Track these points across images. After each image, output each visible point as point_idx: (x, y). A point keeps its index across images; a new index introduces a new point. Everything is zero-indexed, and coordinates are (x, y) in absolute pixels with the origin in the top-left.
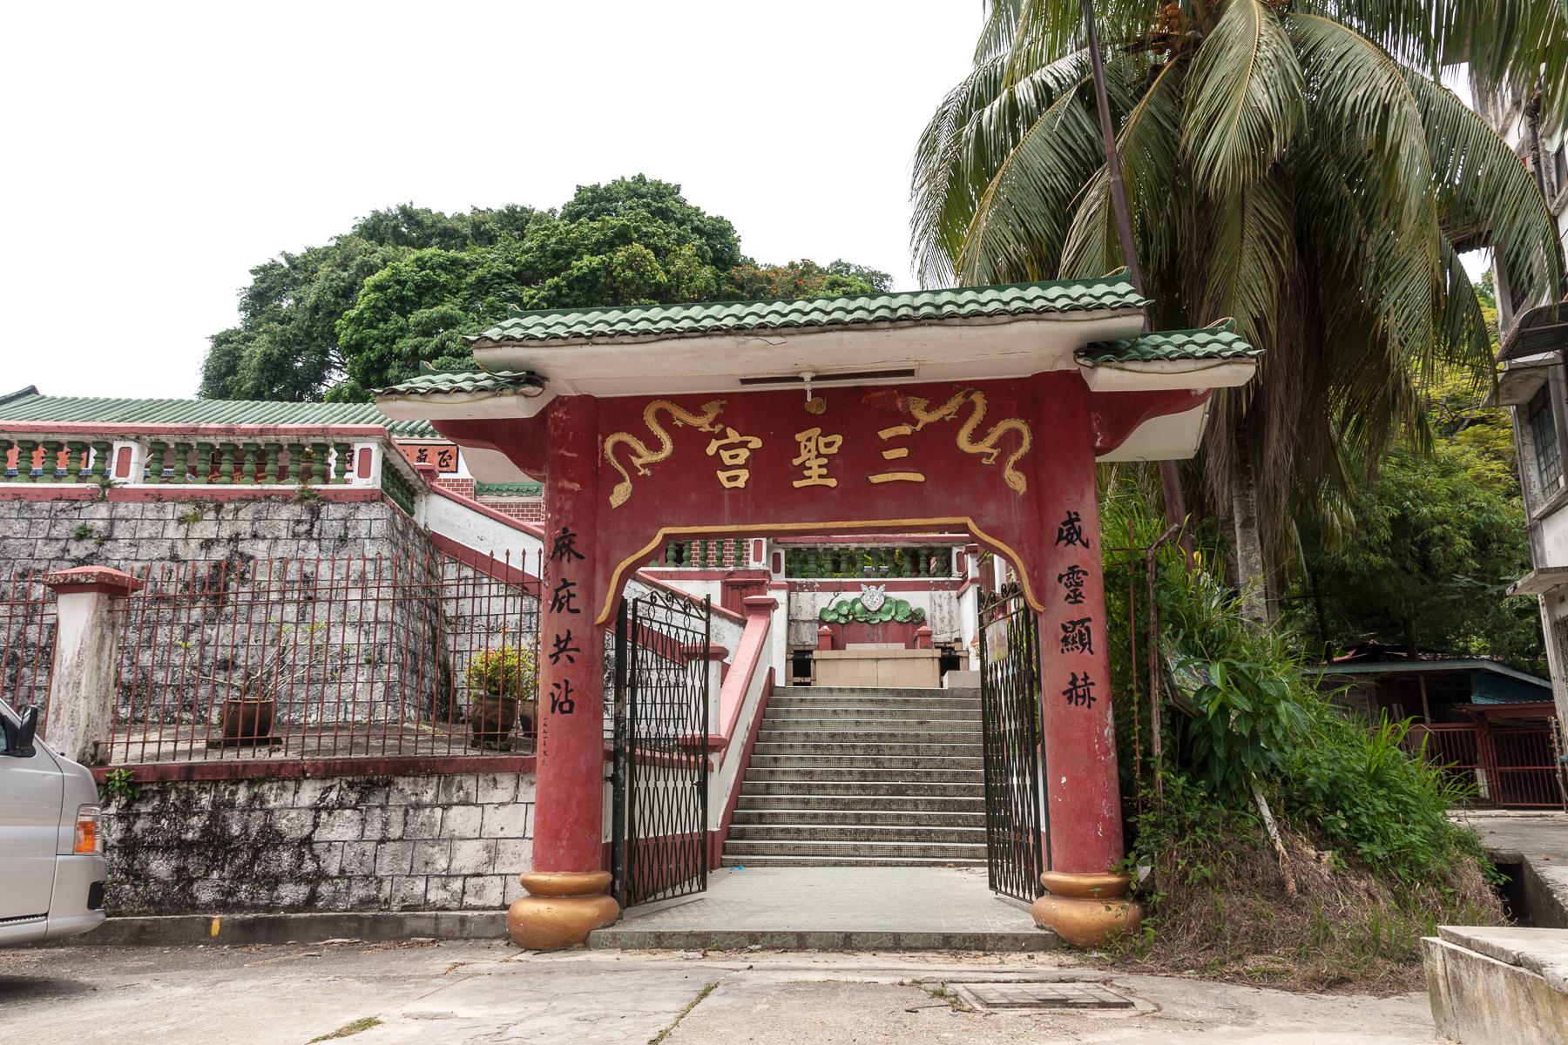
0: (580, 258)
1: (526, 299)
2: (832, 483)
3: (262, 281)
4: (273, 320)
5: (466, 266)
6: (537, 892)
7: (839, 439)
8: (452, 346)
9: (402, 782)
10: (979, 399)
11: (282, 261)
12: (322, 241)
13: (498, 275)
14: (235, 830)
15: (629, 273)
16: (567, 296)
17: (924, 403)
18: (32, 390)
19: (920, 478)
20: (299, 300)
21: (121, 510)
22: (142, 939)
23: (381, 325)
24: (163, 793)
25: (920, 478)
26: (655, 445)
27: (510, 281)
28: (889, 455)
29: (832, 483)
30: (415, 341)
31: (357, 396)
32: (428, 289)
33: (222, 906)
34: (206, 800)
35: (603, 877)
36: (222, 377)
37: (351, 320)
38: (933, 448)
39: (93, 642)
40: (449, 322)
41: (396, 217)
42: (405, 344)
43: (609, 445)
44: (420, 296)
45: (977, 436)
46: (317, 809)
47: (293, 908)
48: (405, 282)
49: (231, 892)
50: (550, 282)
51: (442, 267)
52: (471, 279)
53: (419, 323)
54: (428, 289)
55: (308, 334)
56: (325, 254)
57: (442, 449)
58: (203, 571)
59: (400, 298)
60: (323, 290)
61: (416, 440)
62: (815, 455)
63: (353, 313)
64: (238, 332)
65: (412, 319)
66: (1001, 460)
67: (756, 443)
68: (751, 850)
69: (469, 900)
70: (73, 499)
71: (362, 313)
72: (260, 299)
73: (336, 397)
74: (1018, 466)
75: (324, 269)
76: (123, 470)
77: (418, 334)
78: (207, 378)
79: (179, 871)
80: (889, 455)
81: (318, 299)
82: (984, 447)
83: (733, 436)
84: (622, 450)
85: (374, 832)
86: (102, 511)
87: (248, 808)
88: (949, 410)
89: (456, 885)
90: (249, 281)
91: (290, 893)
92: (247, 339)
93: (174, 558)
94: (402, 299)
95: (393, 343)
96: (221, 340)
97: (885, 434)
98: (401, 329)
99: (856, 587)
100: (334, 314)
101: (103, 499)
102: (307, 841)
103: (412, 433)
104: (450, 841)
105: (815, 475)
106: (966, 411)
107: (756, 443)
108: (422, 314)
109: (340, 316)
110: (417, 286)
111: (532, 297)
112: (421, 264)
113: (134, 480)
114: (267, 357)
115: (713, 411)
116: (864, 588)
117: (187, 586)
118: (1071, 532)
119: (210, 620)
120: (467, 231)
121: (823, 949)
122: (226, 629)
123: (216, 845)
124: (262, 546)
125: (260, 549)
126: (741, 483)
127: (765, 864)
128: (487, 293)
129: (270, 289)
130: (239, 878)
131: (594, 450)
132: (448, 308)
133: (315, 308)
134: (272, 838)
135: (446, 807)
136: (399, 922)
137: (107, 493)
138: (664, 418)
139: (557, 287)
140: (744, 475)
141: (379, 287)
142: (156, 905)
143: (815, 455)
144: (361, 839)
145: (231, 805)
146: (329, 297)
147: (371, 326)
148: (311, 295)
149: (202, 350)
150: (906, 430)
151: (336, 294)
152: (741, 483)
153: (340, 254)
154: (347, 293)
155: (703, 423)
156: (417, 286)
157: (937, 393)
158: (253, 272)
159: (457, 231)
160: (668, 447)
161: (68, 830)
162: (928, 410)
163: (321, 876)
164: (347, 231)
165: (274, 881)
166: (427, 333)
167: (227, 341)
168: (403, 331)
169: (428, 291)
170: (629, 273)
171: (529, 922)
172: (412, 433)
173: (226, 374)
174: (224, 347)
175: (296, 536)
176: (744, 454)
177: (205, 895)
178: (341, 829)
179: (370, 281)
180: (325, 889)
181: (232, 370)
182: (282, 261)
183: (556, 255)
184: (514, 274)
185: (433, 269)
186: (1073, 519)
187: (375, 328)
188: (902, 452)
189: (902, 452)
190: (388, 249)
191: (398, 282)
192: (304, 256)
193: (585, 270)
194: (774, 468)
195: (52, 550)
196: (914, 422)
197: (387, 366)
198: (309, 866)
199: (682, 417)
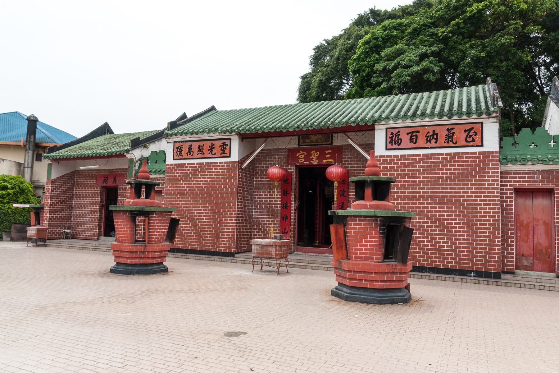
0: (471, 6)
3: (318, 52)
4: (322, 67)
5: (405, 26)
11: (324, 43)
12: (338, 32)
13: (424, 25)
15: (503, 8)
16: (463, 28)
18: (213, 108)
20: (331, 57)
23: (368, 60)
27: (430, 27)
28: (327, 156)
30: (385, 64)
31: (359, 94)
32: (388, 40)
36: (305, 91)
37: (355, 60)
40: (400, 53)
41: (368, 15)
42: (379, 66)
48: (378, 38)
50: (453, 23)
51: (394, 28)
52: (410, 30)
53: (386, 55)
54: (388, 40)
56: (341, 36)
57: (468, 127)
59: (375, 47)
60: (341, 50)
61: (445, 121)
63: (355, 57)
64: (310, 73)
65: (383, 54)
71: (359, 56)
72: (317, 60)
73: (350, 96)
75: (340, 43)
77: (385, 61)
78: (300, 93)
80: (327, 156)
81: (340, 54)
90: (312, 53)
92: (313, 76)
94: (377, 46)
95: (374, 66)
96: (304, 78)
97: (327, 152)
98: (377, 60)
100: (345, 59)
107: (306, 154)
109: (349, 59)
110: (383, 39)
111: (443, 32)
112: (385, 28)
114: (321, 81)
120: (400, 13)
128: (418, 35)
129: (321, 54)
132: (400, 46)
133: (338, 59)
139: (457, 24)
141: (366, 43)
147: (364, 60)
148: (336, 54)
149: (298, 82)
151: (347, 51)
153: (348, 34)
154: (351, 49)
156: (383, 39)
158: (314, 49)
164: (348, 26)
167: (306, 78)
168: (378, 61)
169: (389, 40)
170: (503, 8)
173: (307, 90)
174: (306, 80)
176: (303, 156)
181: (308, 89)
182: (324, 43)
183: (456, 8)
184: (431, 23)
185: (390, 30)
188: (329, 156)
189: (329, 156)
190: (367, 28)
191: (375, 39)
192: (332, 39)
193: (475, 11)
197: (372, 76)
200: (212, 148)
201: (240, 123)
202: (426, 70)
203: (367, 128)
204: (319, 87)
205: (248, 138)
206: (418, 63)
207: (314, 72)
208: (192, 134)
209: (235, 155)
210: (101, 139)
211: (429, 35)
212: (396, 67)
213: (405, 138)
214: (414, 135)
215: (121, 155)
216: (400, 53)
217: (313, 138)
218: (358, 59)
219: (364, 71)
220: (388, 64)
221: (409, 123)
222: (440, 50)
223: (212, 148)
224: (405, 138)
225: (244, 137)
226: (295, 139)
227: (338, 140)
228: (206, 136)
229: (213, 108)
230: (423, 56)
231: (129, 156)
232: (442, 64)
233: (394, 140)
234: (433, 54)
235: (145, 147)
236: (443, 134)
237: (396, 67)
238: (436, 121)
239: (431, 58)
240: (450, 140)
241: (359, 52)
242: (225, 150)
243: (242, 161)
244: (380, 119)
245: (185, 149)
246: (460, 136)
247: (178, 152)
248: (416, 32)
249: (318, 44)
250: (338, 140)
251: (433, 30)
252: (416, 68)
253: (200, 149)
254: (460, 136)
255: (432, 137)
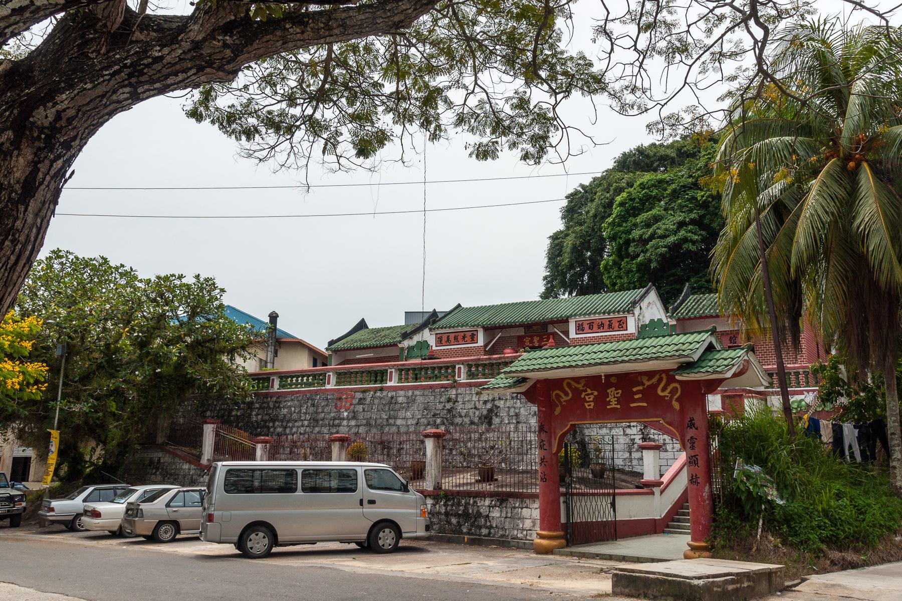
1: (699, 198)
2: (619, 406)
5: (667, 182)
6: (542, 537)
7: (620, 391)
8: (659, 232)
9: (511, 500)
10: (664, 376)
13: (684, 186)
14: (470, 511)
17: (647, 378)
18: (459, 305)
19: (645, 404)
21: (459, 391)
22: (450, 541)
24: (453, 499)
25: (645, 404)
26: (567, 394)
27: (691, 188)
29: (619, 406)
33: (468, 533)
34: (463, 502)
35: (562, 533)
37: (610, 224)
38: (649, 394)
39: (434, 453)
40: (657, 219)
41: (635, 155)
42: (636, 234)
43: (554, 393)
44: (644, 204)
45: (664, 390)
46: (489, 506)
47: (485, 536)
49: (470, 530)
55: (593, 229)
58: (485, 412)
60: (598, 206)
61: (606, 316)
62: (613, 397)
63: (610, 220)
64: (561, 232)
66: (671, 398)
67: (596, 393)
68: (679, 527)
69: (528, 537)
70: (445, 387)
71: (614, 220)
74: (677, 400)
76: (459, 376)
78: (550, 259)
79: (458, 522)
80: (636, 397)
82: (666, 393)
83: (589, 391)
84: (558, 396)
85: (504, 515)
86: (454, 392)
87: (473, 505)
88: (655, 380)
89: (525, 533)
90: (565, 203)
91: (484, 531)
92: (567, 235)
93: (476, 408)
94: (634, 208)
96: (555, 237)
97: (634, 390)
99: (801, 393)
101: (454, 387)
102: (488, 516)
103: (604, 313)
104: (522, 519)
105: (614, 404)
106: (660, 380)
107: (596, 393)
108: (644, 216)
111: (703, 196)
113: (463, 379)
115: (583, 382)
116: (806, 393)
117: (480, 418)
118: (691, 425)
119: (488, 431)
121: (616, 560)
122: (491, 435)
123: (466, 515)
124: (502, 402)
125: (501, 403)
126: (592, 407)
127: (681, 533)
129: (575, 206)
130: (472, 525)
131: (549, 396)
133: (595, 216)
134: (479, 515)
135: (522, 508)
136: (509, 542)
137: (455, 385)
138: (569, 385)
140: (592, 404)
141: (622, 204)
142: (454, 532)
143: (613, 397)
144: (501, 516)
145: (469, 504)
146: (601, 209)
147: (620, 225)
149: (546, 244)
150: (641, 388)
151: (604, 207)
152: (592, 407)
155: (580, 386)
157: (650, 374)
159: (667, 156)
160: (571, 395)
161: (419, 511)
162: (648, 380)
163: (491, 527)
165: (480, 527)
166: (648, 226)
169: (647, 202)
171: (540, 545)
172: (604, 313)
174: (556, 242)
175: (513, 398)
176: (592, 397)
177: (465, 530)
178: (496, 513)
179: (618, 199)
180: (492, 531)
185: (648, 188)
186: (691, 420)
187: (621, 226)
188: (640, 396)
189: (640, 396)
191: (631, 200)
194: (601, 401)
195: (440, 406)
196: (644, 385)
198: (488, 524)
199: (574, 384)
200: (464, 337)
201: (484, 319)
202: (685, 240)
203: (565, 321)
204: (572, 253)
205: (490, 330)
206: (675, 233)
207: (568, 228)
208: (450, 327)
209: (481, 342)
210: (362, 332)
211: (688, 200)
212: (652, 237)
213: (586, 327)
214: (591, 325)
215: (395, 345)
216: (657, 219)
217: (535, 328)
218: (613, 224)
219: (620, 238)
220: (644, 233)
221: (587, 318)
222: (700, 217)
223: (464, 337)
224: (586, 327)
225: (490, 330)
226: (522, 329)
227: (551, 329)
228: (460, 329)
229: (459, 305)
230: (681, 225)
231: (400, 346)
232: (703, 233)
233: (580, 328)
234: (693, 222)
235: (411, 338)
236: (607, 323)
237: (652, 237)
238: (602, 316)
239: (690, 227)
240: (611, 327)
241: (616, 210)
242: (473, 338)
243: (486, 345)
244: (571, 316)
245: (445, 338)
246: (616, 325)
247: (439, 341)
248: (675, 194)
249: (571, 191)
250: (551, 329)
251: (691, 193)
252: (672, 239)
253: (456, 338)
254: (616, 325)
255: (601, 326)
